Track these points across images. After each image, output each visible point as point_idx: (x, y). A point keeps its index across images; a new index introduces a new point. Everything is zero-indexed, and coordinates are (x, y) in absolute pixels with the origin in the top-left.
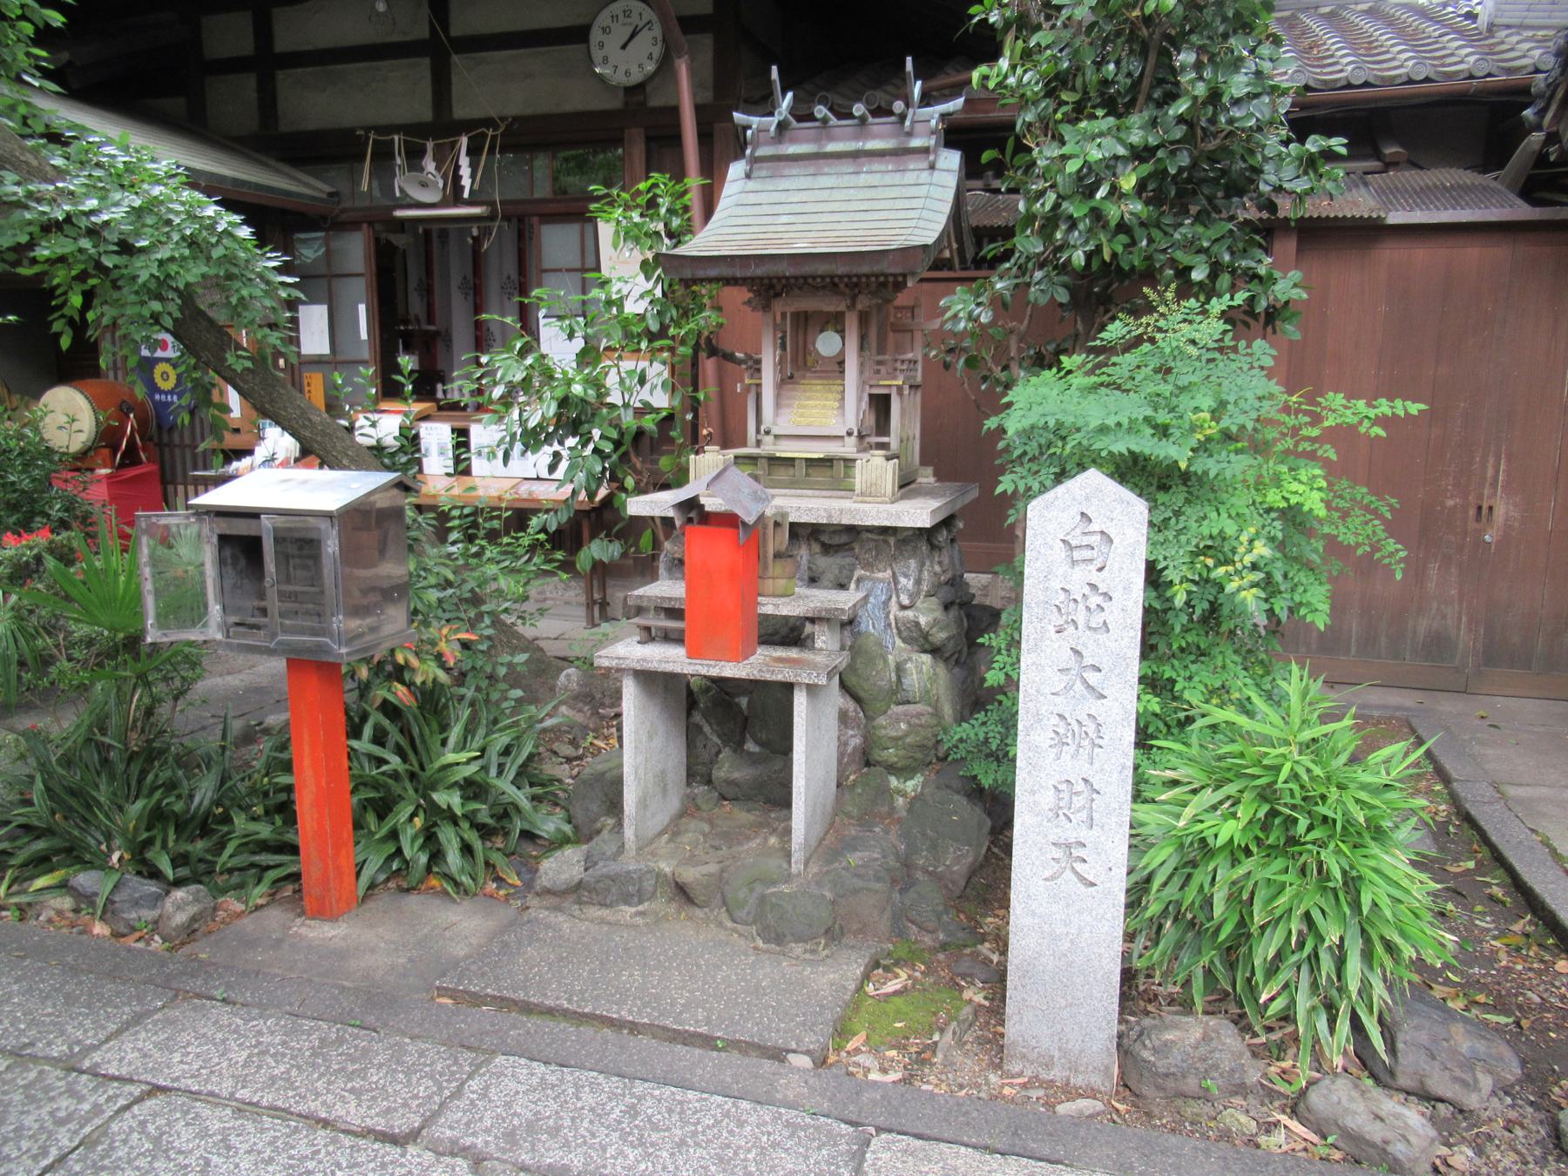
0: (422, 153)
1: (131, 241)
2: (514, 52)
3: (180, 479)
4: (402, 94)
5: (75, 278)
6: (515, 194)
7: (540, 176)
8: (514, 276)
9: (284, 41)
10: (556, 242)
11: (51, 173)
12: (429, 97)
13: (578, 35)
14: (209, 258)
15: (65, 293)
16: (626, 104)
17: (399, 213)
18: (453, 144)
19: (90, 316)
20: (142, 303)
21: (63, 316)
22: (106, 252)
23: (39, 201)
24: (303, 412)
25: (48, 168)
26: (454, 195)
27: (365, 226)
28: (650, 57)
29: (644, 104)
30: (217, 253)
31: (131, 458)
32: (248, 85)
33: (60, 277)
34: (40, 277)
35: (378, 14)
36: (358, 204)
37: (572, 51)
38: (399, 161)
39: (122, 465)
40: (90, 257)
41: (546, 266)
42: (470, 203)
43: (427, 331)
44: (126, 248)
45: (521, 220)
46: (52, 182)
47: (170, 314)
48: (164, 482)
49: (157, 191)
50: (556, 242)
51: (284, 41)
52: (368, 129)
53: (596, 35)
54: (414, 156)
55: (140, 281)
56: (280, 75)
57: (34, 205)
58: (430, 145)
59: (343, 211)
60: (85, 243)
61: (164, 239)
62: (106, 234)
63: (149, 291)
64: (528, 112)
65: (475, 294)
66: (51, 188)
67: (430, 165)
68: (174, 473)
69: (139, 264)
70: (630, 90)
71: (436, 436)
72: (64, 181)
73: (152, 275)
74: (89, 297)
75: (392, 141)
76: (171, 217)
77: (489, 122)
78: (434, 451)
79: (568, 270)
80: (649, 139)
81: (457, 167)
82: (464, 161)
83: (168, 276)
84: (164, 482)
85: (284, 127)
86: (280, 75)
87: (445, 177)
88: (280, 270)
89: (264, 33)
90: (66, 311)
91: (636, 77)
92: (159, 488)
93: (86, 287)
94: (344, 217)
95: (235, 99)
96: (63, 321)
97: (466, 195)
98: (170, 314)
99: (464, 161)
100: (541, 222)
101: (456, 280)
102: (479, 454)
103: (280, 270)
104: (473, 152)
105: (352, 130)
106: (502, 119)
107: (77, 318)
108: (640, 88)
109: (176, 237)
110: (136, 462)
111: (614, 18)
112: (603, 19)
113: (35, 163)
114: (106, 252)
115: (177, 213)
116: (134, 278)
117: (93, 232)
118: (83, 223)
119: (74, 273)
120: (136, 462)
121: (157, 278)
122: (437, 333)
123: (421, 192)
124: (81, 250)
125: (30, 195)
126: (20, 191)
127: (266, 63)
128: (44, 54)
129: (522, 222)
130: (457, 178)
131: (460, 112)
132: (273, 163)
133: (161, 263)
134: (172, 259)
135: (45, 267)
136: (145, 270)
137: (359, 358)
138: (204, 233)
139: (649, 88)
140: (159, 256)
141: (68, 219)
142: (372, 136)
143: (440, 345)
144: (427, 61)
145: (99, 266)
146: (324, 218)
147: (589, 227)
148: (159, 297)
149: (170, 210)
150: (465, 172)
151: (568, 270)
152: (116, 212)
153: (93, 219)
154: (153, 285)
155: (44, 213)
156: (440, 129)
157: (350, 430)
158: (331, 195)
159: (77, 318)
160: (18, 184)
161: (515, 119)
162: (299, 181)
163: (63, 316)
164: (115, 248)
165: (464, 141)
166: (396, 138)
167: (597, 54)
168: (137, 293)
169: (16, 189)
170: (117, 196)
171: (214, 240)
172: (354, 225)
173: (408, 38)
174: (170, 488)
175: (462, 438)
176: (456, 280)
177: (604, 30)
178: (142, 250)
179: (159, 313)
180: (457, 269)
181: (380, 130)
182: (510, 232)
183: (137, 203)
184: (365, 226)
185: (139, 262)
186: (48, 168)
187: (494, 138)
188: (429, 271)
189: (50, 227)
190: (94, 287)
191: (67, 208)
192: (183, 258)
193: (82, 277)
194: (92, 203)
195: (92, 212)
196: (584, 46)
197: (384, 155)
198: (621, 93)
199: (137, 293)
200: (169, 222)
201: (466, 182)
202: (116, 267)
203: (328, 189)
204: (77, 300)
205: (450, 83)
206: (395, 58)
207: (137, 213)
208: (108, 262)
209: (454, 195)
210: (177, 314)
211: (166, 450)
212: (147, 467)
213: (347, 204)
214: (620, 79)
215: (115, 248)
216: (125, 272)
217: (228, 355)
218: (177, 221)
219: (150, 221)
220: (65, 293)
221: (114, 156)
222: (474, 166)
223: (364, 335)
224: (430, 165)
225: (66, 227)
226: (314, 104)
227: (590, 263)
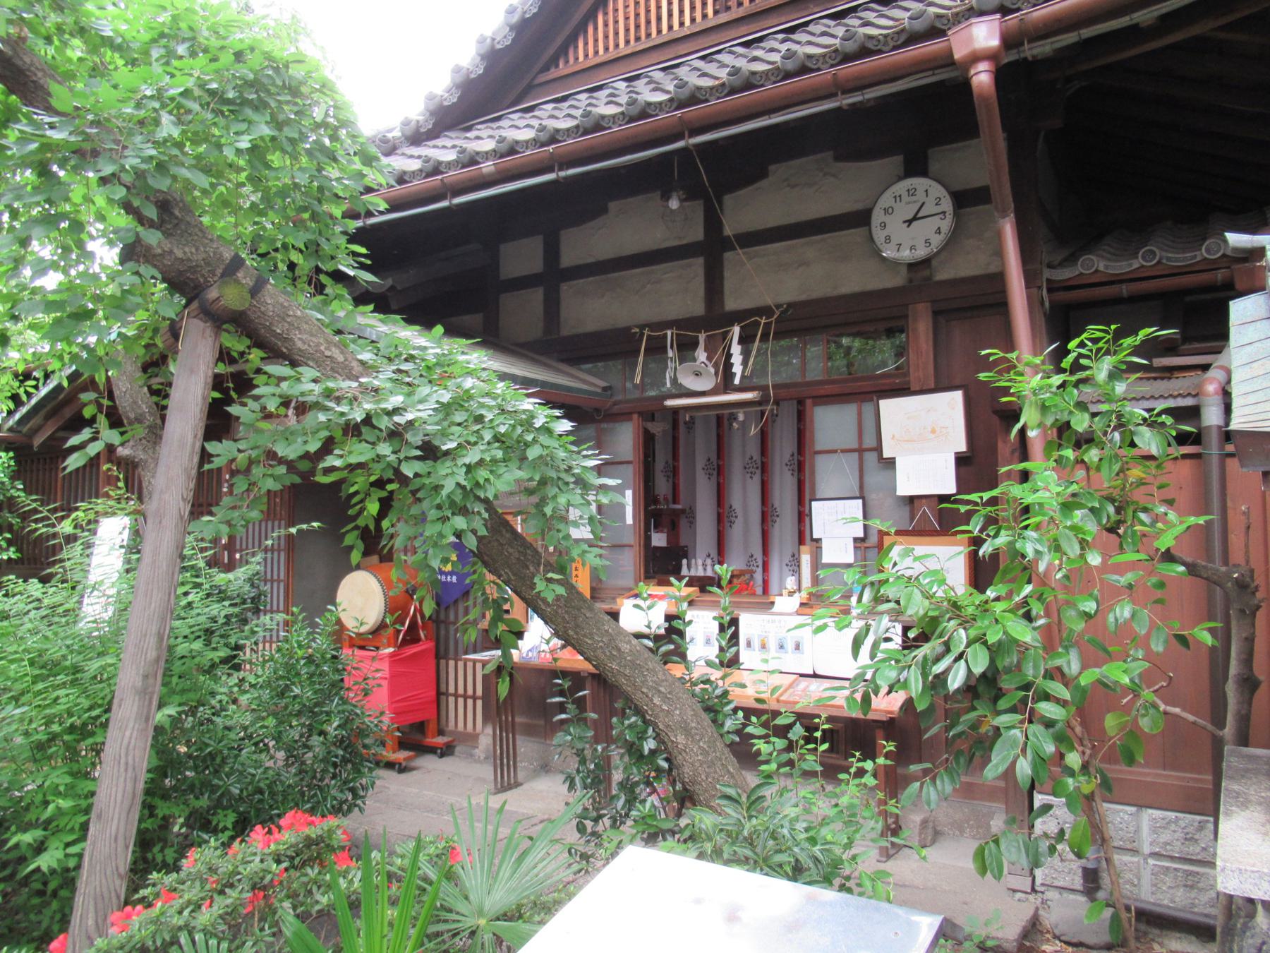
0: (695, 345)
1: (436, 443)
2: (789, 243)
3: (452, 654)
4: (679, 292)
5: (373, 484)
6: (784, 378)
7: (813, 361)
8: (757, 457)
9: (568, 259)
10: (832, 424)
11: (357, 368)
12: (702, 292)
13: (861, 218)
14: (523, 459)
15: (362, 501)
16: (911, 281)
17: (670, 403)
18: (725, 336)
19: (385, 524)
20: (444, 519)
21: (356, 528)
22: (407, 458)
23: (338, 400)
24: (612, 639)
25: (354, 364)
26: (726, 383)
27: (635, 416)
28: (939, 231)
29: (929, 278)
30: (533, 453)
31: (412, 637)
32: (536, 297)
33: (359, 483)
34: (338, 485)
35: (672, 211)
36: (629, 397)
37: (853, 235)
38: (670, 354)
39: (404, 642)
40: (389, 465)
41: (818, 448)
42: (741, 389)
43: (674, 510)
44: (430, 452)
45: (801, 402)
46: (356, 378)
47: (474, 532)
48: (438, 657)
49: (469, 383)
50: (832, 424)
51: (568, 259)
52: (642, 327)
53: (877, 217)
54: (686, 348)
55: (444, 492)
56: (564, 287)
57: (331, 404)
58: (702, 337)
59: (615, 404)
60: (385, 449)
61: (473, 439)
62: (409, 436)
63: (453, 504)
64: (803, 297)
65: (719, 474)
66: (355, 384)
67: (701, 355)
68: (447, 649)
69: (443, 472)
70: (913, 266)
71: (702, 629)
72: (368, 375)
73: (458, 484)
74: (386, 505)
75: (665, 336)
76: (483, 412)
77: (765, 311)
78: (700, 640)
79: (843, 451)
80: (936, 314)
81: (729, 356)
82: (736, 349)
83: (477, 484)
84: (438, 657)
85: (565, 332)
86: (564, 287)
87: (716, 366)
88: (599, 470)
89: (552, 252)
90: (361, 522)
91: (921, 253)
92: (433, 662)
93: (384, 494)
94: (616, 409)
95: (524, 311)
96: (356, 533)
97: (737, 381)
98: (474, 532)
99: (736, 349)
100: (815, 404)
101: (700, 463)
102: (749, 644)
103: (599, 470)
104: (745, 340)
105: (628, 329)
106: (778, 306)
107: (372, 527)
108: (926, 262)
109: (488, 436)
110: (416, 640)
111: (898, 198)
112: (886, 200)
113: (341, 358)
114: (407, 458)
115: (490, 408)
116: (437, 488)
117: (395, 435)
118: (384, 423)
119: (373, 478)
120: (416, 640)
121: (463, 488)
122: (683, 511)
123: (693, 381)
124: (379, 458)
125: (328, 394)
126: (317, 388)
127: (553, 277)
128: (363, 251)
129: (799, 402)
130: (728, 365)
131: (732, 303)
132: (554, 364)
133: (469, 468)
134: (481, 462)
135: (345, 474)
136: (450, 477)
137: (625, 542)
138: (519, 430)
139: (934, 263)
140: (467, 461)
141: (368, 421)
142: (646, 332)
143: (683, 522)
144: (701, 260)
145: (397, 472)
146: (597, 410)
147: (868, 408)
148: (464, 511)
149: (482, 405)
150: (737, 359)
151: (843, 451)
152: (420, 411)
153: (397, 419)
154: (458, 498)
155: (342, 414)
156: (714, 320)
157: (615, 616)
158: (605, 389)
159: (372, 527)
160: (315, 381)
161: (790, 305)
162: (572, 376)
163: (356, 528)
164: (418, 453)
165: (736, 330)
166: (669, 333)
167: (879, 236)
168: (439, 507)
169: (312, 386)
170: (425, 390)
171: (529, 438)
172: (623, 416)
173: (684, 242)
174: (443, 662)
175: (730, 628)
176: (700, 463)
177: (886, 211)
178: (447, 453)
179: (462, 531)
180: (702, 447)
181: (654, 326)
182: (789, 410)
183: (446, 397)
184: (635, 416)
185: (443, 468)
186: (354, 364)
187: (767, 325)
188: (675, 456)
189: (353, 430)
190: (392, 492)
191: (367, 406)
192: (494, 461)
193: (380, 484)
194: (397, 400)
195: (397, 411)
196: (861, 231)
197: (657, 348)
198: (904, 270)
199: (439, 507)
200: (479, 419)
201: (737, 369)
202: (417, 475)
203: (605, 384)
204: (373, 508)
205: (722, 278)
206: (666, 261)
207: (445, 409)
208: (408, 470)
209: (726, 383)
210: (483, 532)
211: (442, 626)
212: (425, 645)
213: (619, 397)
214: (906, 255)
215: (418, 453)
216: (427, 481)
217: (536, 580)
218: (489, 416)
219: (459, 417)
220: (362, 501)
221: (426, 348)
222: (746, 354)
223: (629, 520)
224: (701, 355)
225: (364, 429)
226: (590, 310)
227: (869, 442)
